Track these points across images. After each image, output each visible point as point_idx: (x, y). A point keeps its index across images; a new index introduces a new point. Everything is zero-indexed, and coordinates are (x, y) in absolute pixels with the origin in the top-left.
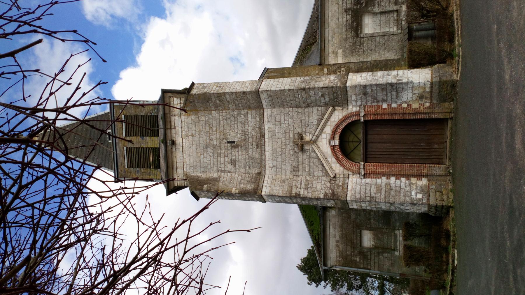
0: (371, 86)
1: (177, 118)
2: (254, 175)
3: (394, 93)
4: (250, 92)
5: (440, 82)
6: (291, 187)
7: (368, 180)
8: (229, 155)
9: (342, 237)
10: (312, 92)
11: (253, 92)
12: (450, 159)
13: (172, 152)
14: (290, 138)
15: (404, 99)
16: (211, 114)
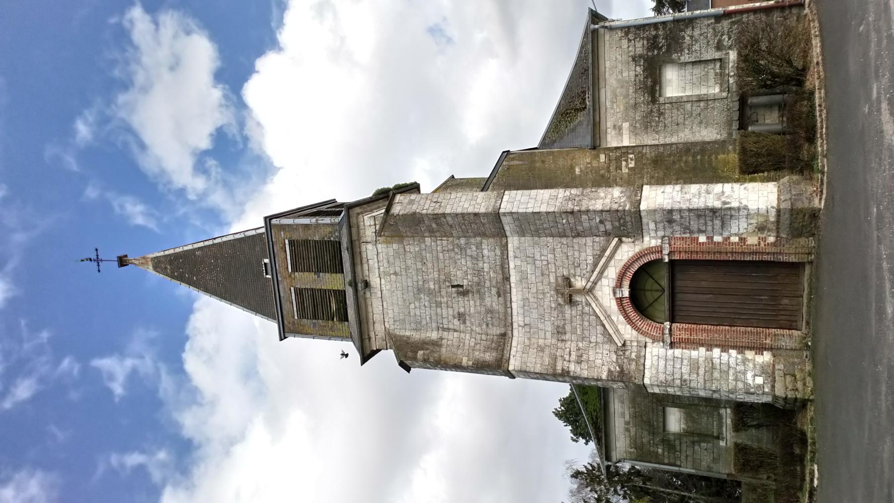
0: (680, 211)
1: (370, 246)
2: (495, 338)
3: (718, 222)
4: (486, 215)
5: (792, 210)
6: (555, 359)
7: (678, 352)
8: (455, 305)
9: (634, 416)
10: (584, 217)
11: (491, 214)
12: (808, 323)
13: (365, 299)
14: (549, 283)
15: (734, 230)
16: (424, 242)
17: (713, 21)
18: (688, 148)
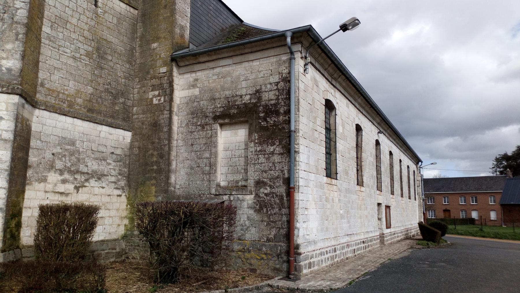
17: (286, 176)
18: (165, 157)
